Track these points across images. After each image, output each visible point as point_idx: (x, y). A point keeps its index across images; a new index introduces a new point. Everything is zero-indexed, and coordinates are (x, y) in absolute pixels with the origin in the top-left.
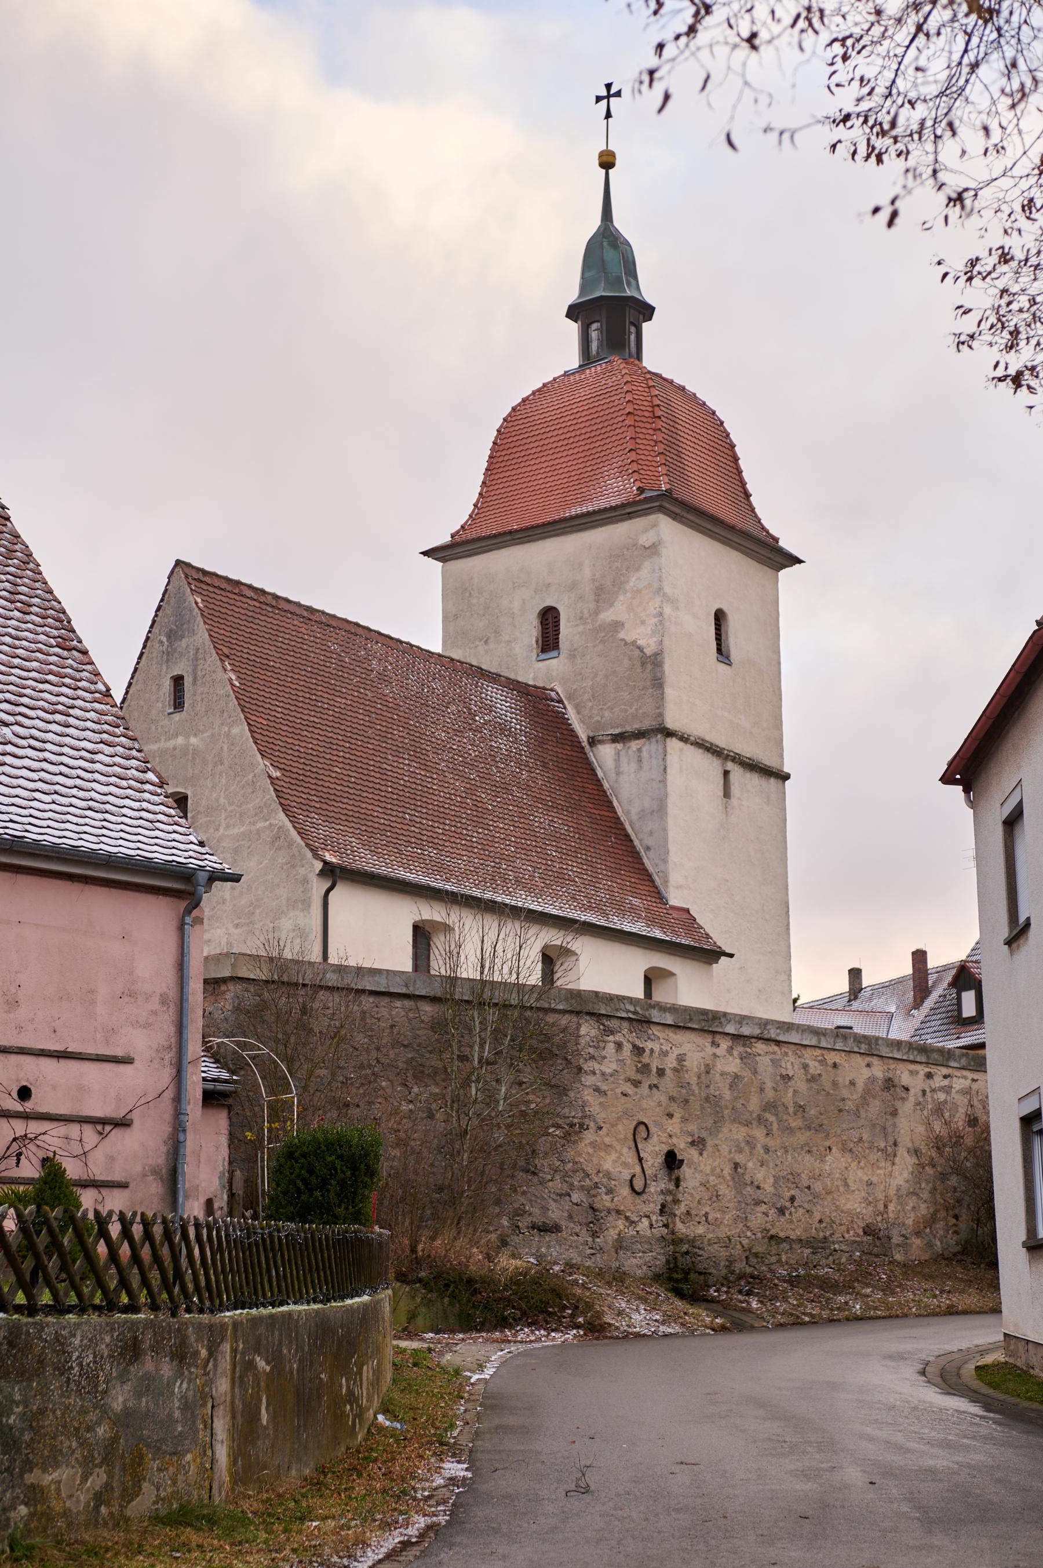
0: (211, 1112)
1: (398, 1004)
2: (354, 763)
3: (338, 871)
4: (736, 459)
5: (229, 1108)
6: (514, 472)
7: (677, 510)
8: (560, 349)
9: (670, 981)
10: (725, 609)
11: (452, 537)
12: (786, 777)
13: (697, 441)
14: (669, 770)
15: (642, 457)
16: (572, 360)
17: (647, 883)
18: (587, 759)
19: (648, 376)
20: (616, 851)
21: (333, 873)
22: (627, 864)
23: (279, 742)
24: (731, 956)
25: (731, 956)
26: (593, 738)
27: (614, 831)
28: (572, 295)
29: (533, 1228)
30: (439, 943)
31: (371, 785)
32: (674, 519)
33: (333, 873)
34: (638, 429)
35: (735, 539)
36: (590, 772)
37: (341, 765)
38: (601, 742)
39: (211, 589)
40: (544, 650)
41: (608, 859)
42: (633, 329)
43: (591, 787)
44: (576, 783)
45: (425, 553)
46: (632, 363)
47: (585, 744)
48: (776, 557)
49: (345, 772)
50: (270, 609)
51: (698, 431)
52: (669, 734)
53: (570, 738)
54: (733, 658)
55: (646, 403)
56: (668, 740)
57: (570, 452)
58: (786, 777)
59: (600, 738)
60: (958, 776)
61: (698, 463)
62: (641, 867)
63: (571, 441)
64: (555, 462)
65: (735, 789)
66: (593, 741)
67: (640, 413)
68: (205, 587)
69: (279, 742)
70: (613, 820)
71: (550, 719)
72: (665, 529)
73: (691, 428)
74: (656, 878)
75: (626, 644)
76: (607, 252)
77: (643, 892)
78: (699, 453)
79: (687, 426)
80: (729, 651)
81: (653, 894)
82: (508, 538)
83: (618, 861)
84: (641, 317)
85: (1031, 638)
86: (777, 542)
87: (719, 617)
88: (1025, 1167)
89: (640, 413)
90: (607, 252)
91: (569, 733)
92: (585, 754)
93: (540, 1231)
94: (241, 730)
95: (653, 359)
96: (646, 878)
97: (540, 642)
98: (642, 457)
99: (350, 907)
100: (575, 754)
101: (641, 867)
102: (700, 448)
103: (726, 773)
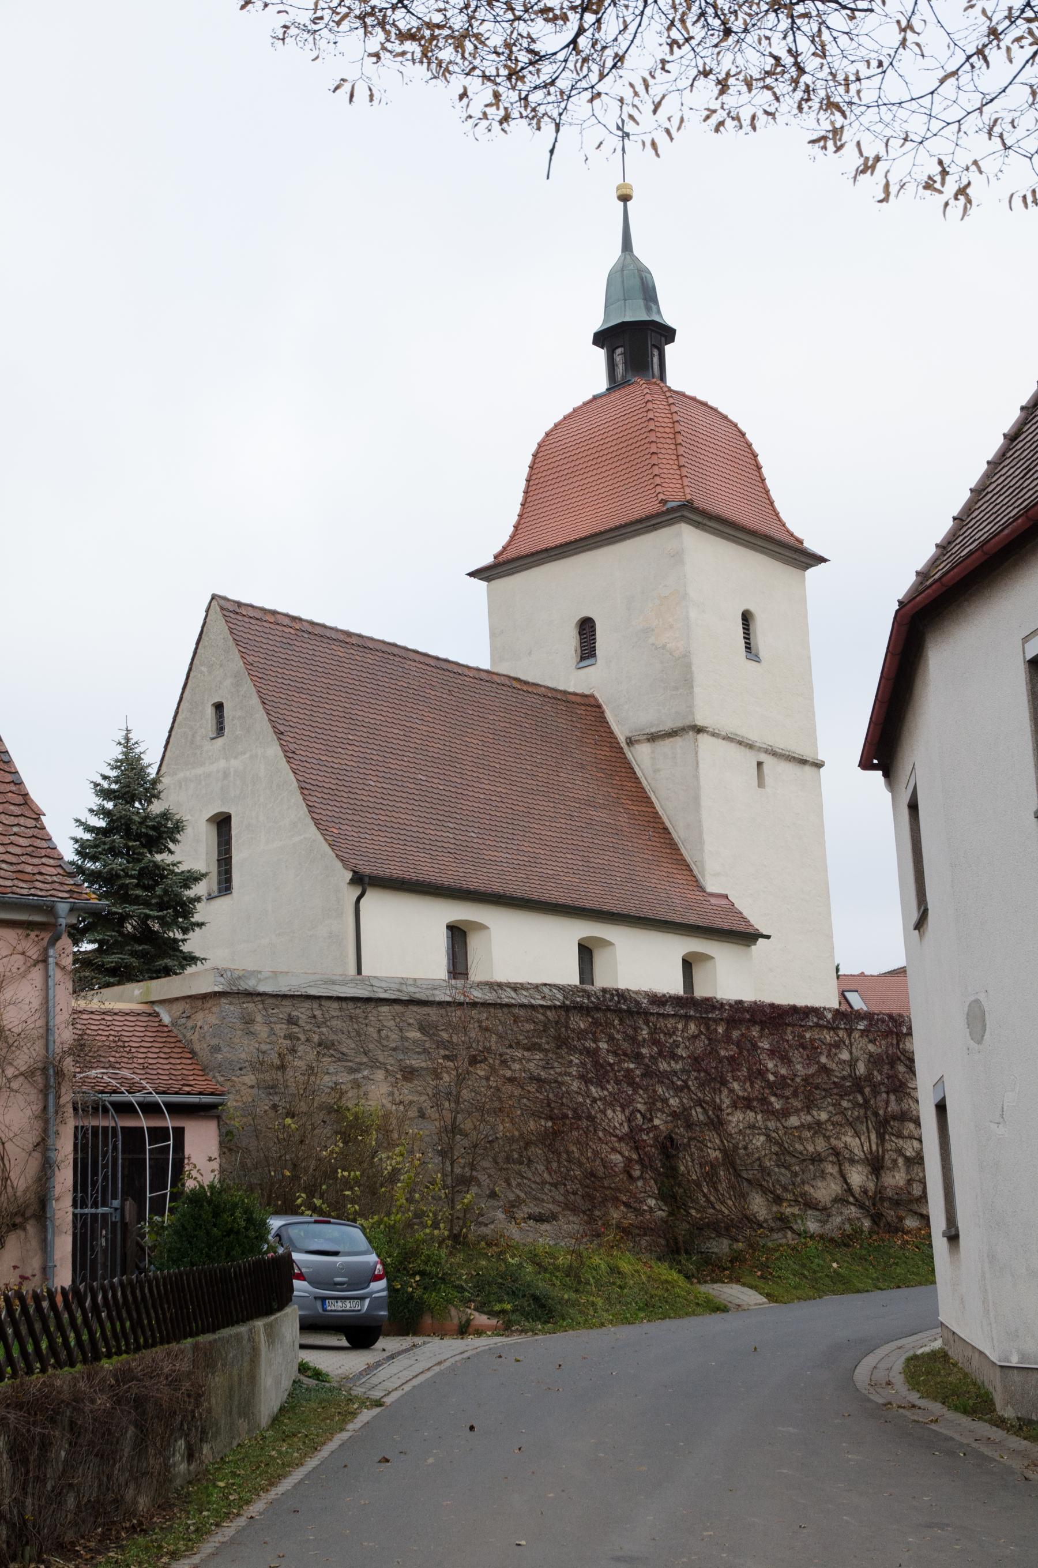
0: (895, 1010)
1: (385, 1009)
2: (389, 775)
3: (367, 880)
4: (759, 468)
5: (218, 1118)
6: (549, 493)
7: (699, 519)
8: (590, 373)
9: (709, 964)
10: (752, 609)
11: (495, 558)
12: (819, 765)
13: (719, 453)
14: (701, 765)
15: (665, 471)
16: (600, 383)
17: (685, 873)
18: (626, 758)
19: (668, 394)
20: (654, 844)
21: (362, 881)
22: (665, 855)
23: (312, 760)
24: (768, 937)
25: (768, 937)
26: (630, 738)
27: (652, 825)
28: (597, 323)
29: (529, 1218)
30: (475, 943)
31: (404, 795)
32: (697, 527)
33: (362, 881)
34: (660, 445)
35: (759, 543)
36: (629, 770)
37: (375, 779)
38: (638, 741)
39: (247, 620)
40: (583, 658)
41: (646, 851)
42: (656, 352)
43: (629, 784)
44: (615, 782)
45: (471, 574)
46: (655, 383)
47: (624, 745)
48: (802, 558)
49: (379, 785)
50: (306, 636)
51: (720, 443)
52: (699, 730)
53: (609, 740)
54: (761, 655)
55: (666, 420)
56: (700, 736)
57: (599, 471)
58: (819, 765)
59: (637, 738)
60: (875, 761)
61: (740, 472)
62: (679, 857)
63: (599, 460)
64: (586, 481)
65: (769, 779)
66: (630, 742)
67: (661, 429)
68: (240, 618)
69: (312, 760)
70: (652, 815)
71: (589, 722)
72: (687, 537)
73: (713, 441)
74: (693, 867)
75: (656, 649)
76: (632, 281)
77: (681, 882)
78: (721, 464)
79: (709, 439)
80: (757, 649)
81: (691, 883)
82: (545, 555)
83: (655, 853)
84: (663, 339)
85: (895, 618)
86: (802, 543)
87: (746, 618)
88: (942, 1148)
89: (661, 429)
90: (632, 281)
91: (609, 735)
92: (624, 753)
93: (537, 1221)
94: (274, 751)
95: (675, 380)
96: (684, 868)
97: (579, 651)
98: (665, 471)
99: (383, 912)
100: (613, 754)
101: (679, 857)
102: (722, 459)
103: (760, 764)
